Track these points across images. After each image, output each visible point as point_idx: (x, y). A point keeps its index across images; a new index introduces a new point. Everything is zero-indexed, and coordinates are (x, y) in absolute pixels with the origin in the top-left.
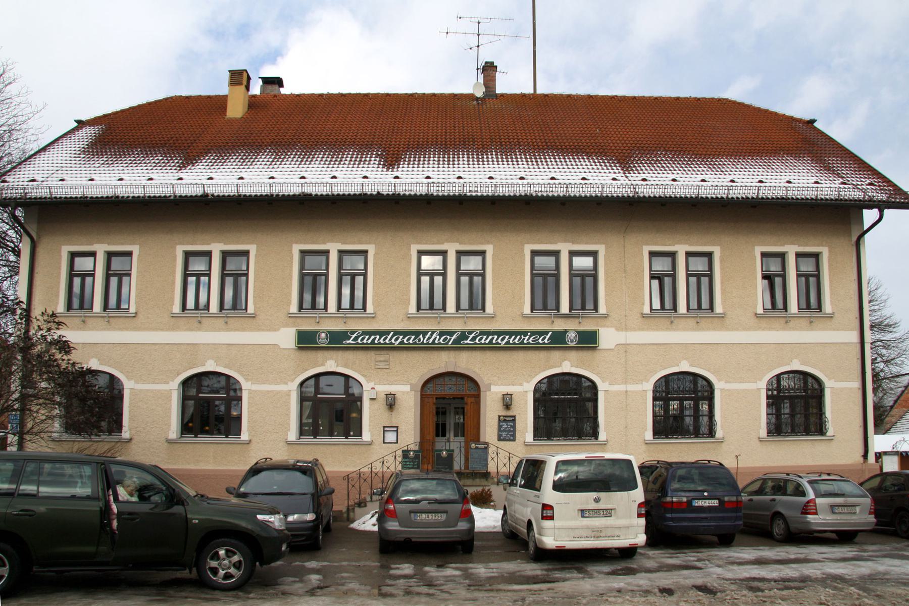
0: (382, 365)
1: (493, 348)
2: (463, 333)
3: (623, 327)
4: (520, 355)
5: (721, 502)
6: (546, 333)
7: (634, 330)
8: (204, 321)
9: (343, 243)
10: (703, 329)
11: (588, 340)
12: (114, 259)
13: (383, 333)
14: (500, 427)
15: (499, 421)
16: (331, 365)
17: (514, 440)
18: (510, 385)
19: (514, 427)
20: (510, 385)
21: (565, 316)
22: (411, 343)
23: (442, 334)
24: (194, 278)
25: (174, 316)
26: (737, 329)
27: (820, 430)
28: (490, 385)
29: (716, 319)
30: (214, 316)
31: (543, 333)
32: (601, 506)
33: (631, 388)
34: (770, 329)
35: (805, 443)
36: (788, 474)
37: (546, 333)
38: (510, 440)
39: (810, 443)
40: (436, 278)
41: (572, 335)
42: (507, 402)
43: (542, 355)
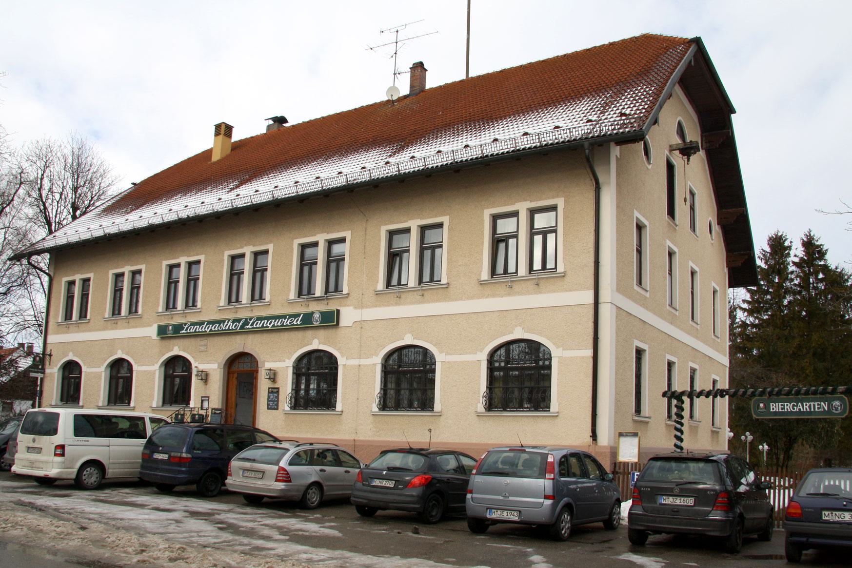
0: (203, 348)
1: (264, 331)
2: (246, 319)
3: (361, 306)
4: (286, 335)
5: (170, 456)
6: (299, 315)
7: (368, 307)
8: (403, 296)
9: (189, 256)
10: (428, 302)
11: (331, 320)
12: (499, 222)
13: (201, 324)
14: (269, 397)
15: (269, 392)
16: (315, 345)
17: (277, 409)
18: (278, 360)
19: (278, 397)
20: (278, 360)
21: (319, 299)
22: (218, 331)
23: (234, 321)
24: (540, 236)
25: (482, 283)
26: (461, 299)
27: (427, 404)
28: (264, 362)
29: (441, 291)
30: (413, 290)
31: (296, 316)
32: (36, 445)
33: (364, 362)
34: (494, 295)
35: (526, 419)
36: (311, 444)
37: (299, 315)
38: (274, 409)
39: (511, 418)
40: (549, 235)
41: (317, 316)
42: (273, 376)
43: (299, 335)
